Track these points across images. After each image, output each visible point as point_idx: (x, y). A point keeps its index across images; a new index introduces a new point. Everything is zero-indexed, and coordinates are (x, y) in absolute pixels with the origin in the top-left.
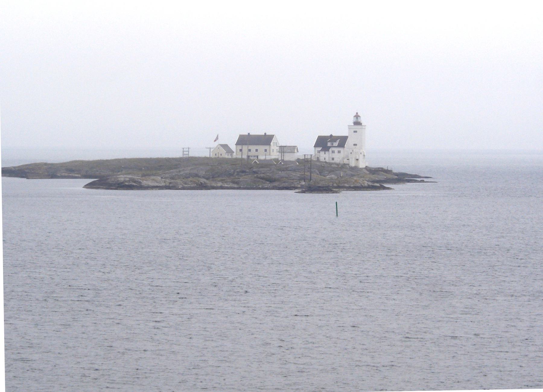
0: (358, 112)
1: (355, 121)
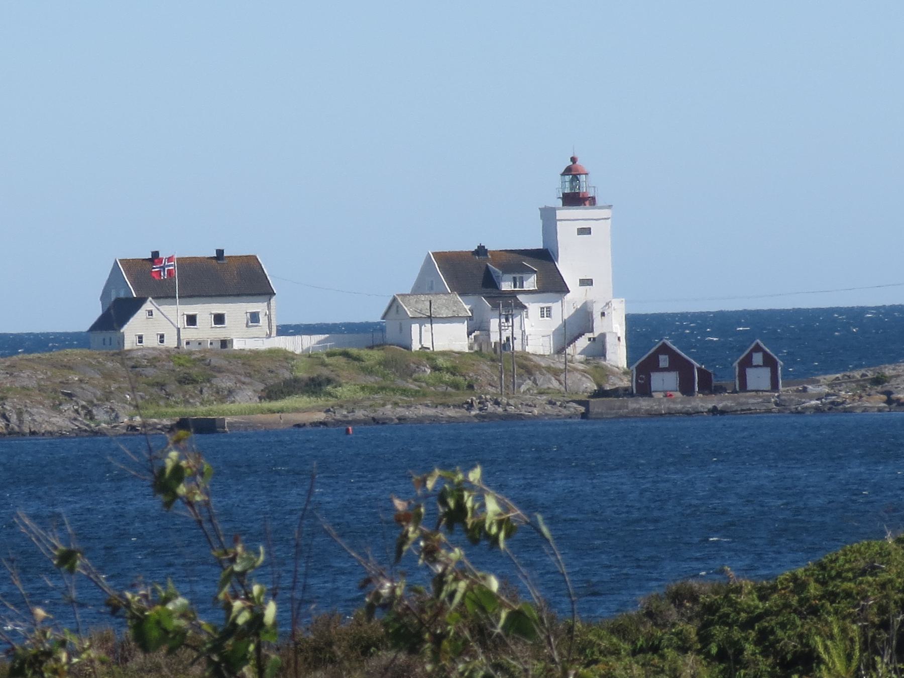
0: (576, 155)
1: (567, 191)
